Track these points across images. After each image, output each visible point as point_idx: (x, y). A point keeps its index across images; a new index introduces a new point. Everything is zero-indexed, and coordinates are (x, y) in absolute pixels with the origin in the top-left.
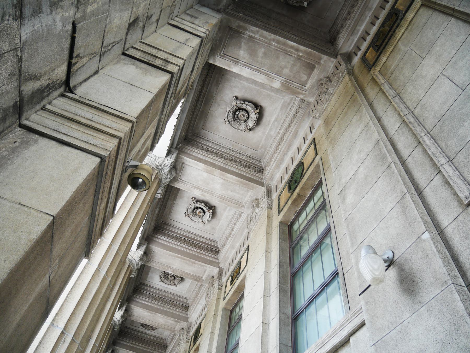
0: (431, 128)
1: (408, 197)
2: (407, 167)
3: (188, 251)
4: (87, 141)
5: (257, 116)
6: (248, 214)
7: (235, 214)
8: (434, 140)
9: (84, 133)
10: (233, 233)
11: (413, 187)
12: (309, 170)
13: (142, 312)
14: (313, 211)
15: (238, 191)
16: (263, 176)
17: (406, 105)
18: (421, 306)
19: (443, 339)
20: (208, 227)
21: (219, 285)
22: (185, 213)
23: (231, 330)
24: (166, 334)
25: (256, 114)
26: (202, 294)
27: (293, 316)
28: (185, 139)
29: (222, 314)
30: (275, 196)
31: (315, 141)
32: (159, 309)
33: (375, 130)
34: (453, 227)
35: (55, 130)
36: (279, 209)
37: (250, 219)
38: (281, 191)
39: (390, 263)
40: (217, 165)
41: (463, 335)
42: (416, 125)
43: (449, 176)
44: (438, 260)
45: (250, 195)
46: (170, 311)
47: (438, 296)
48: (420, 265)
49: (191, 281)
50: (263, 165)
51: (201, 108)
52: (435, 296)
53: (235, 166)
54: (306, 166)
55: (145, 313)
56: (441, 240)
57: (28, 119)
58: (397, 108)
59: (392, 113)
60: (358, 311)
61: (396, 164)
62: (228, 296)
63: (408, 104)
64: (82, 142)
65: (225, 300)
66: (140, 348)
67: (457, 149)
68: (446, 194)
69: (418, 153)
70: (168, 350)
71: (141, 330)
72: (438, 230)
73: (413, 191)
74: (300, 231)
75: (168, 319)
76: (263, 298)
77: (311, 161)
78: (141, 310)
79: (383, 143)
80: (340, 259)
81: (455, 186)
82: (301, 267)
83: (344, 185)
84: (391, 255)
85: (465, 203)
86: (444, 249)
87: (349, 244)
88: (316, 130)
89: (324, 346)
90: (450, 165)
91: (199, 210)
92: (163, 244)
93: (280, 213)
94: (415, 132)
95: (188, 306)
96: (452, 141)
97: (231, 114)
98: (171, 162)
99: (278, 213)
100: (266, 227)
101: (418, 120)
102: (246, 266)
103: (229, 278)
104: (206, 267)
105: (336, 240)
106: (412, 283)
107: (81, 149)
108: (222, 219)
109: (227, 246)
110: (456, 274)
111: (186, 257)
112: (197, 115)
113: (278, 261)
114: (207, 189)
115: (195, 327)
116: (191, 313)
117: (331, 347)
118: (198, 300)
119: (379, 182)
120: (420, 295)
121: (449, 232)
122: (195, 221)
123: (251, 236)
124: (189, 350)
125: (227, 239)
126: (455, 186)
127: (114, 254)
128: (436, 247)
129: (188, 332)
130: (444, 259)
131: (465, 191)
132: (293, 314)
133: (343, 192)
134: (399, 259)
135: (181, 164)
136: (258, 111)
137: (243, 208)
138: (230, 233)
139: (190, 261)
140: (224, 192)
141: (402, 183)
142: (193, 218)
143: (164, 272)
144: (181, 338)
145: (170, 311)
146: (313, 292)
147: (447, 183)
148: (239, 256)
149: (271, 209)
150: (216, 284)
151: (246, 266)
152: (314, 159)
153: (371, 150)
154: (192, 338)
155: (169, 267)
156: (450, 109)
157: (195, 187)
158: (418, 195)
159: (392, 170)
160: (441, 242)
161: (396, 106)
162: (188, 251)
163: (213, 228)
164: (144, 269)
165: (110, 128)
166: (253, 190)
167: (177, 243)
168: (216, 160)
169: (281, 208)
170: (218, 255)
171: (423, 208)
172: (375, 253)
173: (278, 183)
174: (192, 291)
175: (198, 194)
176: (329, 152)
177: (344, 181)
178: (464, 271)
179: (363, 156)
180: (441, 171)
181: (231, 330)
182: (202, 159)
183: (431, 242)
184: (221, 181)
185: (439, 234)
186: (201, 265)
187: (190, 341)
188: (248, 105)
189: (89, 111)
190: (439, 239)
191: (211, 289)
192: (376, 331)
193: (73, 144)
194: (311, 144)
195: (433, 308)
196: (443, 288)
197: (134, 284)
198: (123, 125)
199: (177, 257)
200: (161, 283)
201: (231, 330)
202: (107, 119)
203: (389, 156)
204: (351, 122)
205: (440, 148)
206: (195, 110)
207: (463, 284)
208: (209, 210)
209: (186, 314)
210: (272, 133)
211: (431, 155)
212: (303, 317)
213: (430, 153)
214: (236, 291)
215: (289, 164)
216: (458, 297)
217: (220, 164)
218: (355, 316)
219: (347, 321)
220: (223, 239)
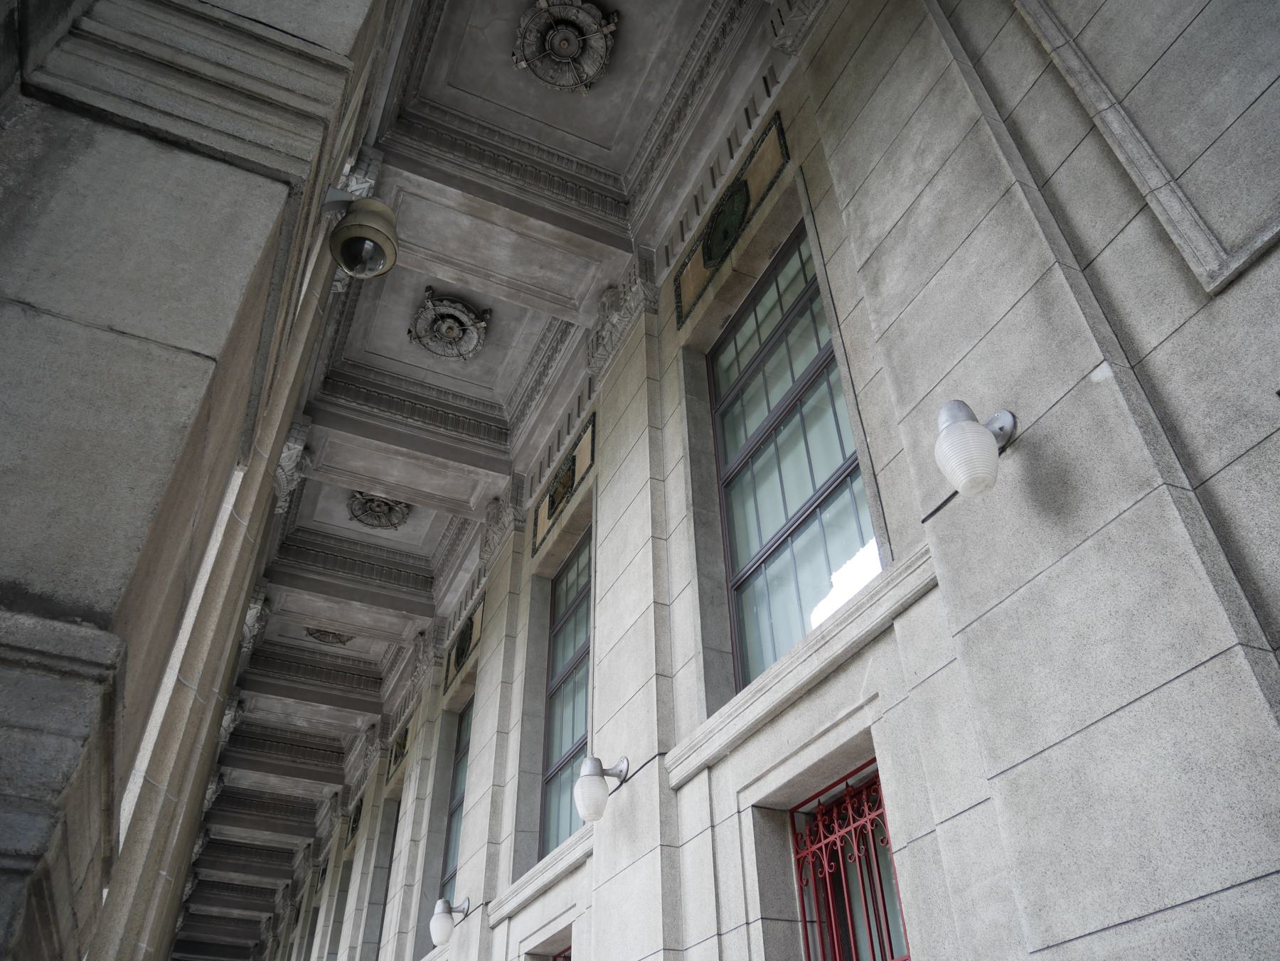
0: (1127, 87)
1: (1059, 275)
2: (1053, 195)
4: (237, 134)
5: (609, 43)
6: (587, 329)
7: (548, 330)
8: (1133, 121)
9: (220, 110)
10: (546, 381)
11: (1069, 250)
12: (764, 202)
14: (778, 315)
15: (559, 266)
16: (627, 220)
17: (1057, 17)
18: (1084, 538)
19: (1132, 609)
20: (475, 368)
21: (515, 520)
22: (410, 332)
23: (557, 629)
24: (377, 650)
25: (606, 36)
27: (733, 582)
28: (399, 117)
30: (664, 276)
31: (779, 118)
33: (968, 90)
34: (1170, 351)
35: (135, 102)
36: (678, 313)
37: (595, 342)
38: (681, 263)
39: (1007, 441)
41: (1182, 597)
42: (1086, 77)
43: (1170, 221)
44: (1130, 430)
45: (594, 277)
46: (384, 592)
47: (1127, 513)
48: (1084, 445)
49: (435, 512)
51: (442, 19)
52: (1120, 515)
53: (550, 193)
54: (755, 189)
55: (319, 604)
56: (1137, 382)
57: (42, 67)
58: (1033, 27)
59: (1016, 40)
60: (918, 559)
61: (1026, 188)
62: (543, 544)
63: (1063, 16)
64: (224, 138)
65: (536, 556)
66: (312, 688)
67: (1196, 148)
68: (1157, 267)
69: (1088, 156)
70: (385, 689)
71: (310, 645)
72: (1130, 358)
73: (1070, 260)
74: (742, 369)
77: (769, 178)
78: (307, 597)
79: (992, 129)
80: (863, 438)
81: (1185, 246)
82: (747, 463)
83: (875, 245)
84: (1007, 422)
85: (1208, 290)
86: (1144, 405)
87: (893, 398)
88: (783, 88)
89: (827, 645)
90: (1173, 191)
91: (450, 322)
92: (352, 420)
93: (683, 323)
94: (1082, 100)
95: (433, 578)
96: (1183, 125)
97: (532, 38)
98: (366, 185)
99: (678, 323)
100: (645, 363)
101: (1090, 63)
102: (591, 466)
103: (542, 500)
104: (478, 474)
105: (851, 389)
106: (1062, 487)
107: (227, 158)
108: (514, 344)
109: (532, 417)
110: (1171, 461)
111: (420, 451)
112: (431, 40)
113: (684, 449)
114: (473, 262)
115: (456, 628)
116: (442, 594)
117: (846, 646)
118: (459, 561)
119: (979, 237)
120: (1081, 513)
121: (1159, 361)
123: (599, 387)
124: (446, 683)
125: (531, 398)
126: (1185, 246)
128: (1128, 400)
129: (438, 640)
130: (1144, 427)
131: (1208, 259)
132: (731, 578)
133: (874, 264)
134: (1029, 430)
135: (394, 192)
136: (612, 27)
137: (574, 313)
138: (539, 382)
139: (432, 462)
140: (520, 270)
141: (1044, 240)
143: (361, 493)
144: (421, 657)
145: (384, 592)
146: (784, 521)
147: (1163, 238)
148: (568, 440)
149: (656, 312)
150: (508, 518)
151: (591, 466)
152: (780, 171)
153: (953, 145)
154: (450, 655)
155: (375, 481)
156: (1184, 34)
157: (438, 258)
158: (1083, 271)
159: (1015, 204)
160: (1138, 386)
161: (1029, 19)
162: (424, 435)
165: (288, 90)
166: (601, 261)
167: (393, 415)
168: (496, 179)
169: (685, 309)
171: (1095, 303)
172: (973, 418)
173: (671, 241)
175: (445, 276)
176: (827, 151)
177: (874, 232)
178: (1189, 455)
179: (930, 163)
180: (1149, 207)
181: (560, 625)
182: (455, 177)
183: (1117, 388)
184: (512, 238)
185: (1132, 368)
186: (462, 470)
187: (445, 663)
188: (583, 9)
189: (213, 36)
190: (1133, 381)
191: (495, 530)
192: (968, 601)
193: (200, 144)
194: (770, 129)
195: (1113, 542)
196: (1140, 496)
197: (280, 531)
198: (323, 82)
199: (397, 453)
200: (355, 525)
201: (557, 629)
202: (272, 63)
203: (1007, 164)
204: (895, 65)
205: (1150, 144)
206: (424, 25)
207: (1186, 484)
209: (428, 598)
210: (652, 95)
211: (1124, 164)
212: (759, 582)
213: (1122, 158)
214: (566, 531)
215: (702, 187)
216: (1177, 513)
218: (909, 572)
219: (888, 583)
220: (517, 399)
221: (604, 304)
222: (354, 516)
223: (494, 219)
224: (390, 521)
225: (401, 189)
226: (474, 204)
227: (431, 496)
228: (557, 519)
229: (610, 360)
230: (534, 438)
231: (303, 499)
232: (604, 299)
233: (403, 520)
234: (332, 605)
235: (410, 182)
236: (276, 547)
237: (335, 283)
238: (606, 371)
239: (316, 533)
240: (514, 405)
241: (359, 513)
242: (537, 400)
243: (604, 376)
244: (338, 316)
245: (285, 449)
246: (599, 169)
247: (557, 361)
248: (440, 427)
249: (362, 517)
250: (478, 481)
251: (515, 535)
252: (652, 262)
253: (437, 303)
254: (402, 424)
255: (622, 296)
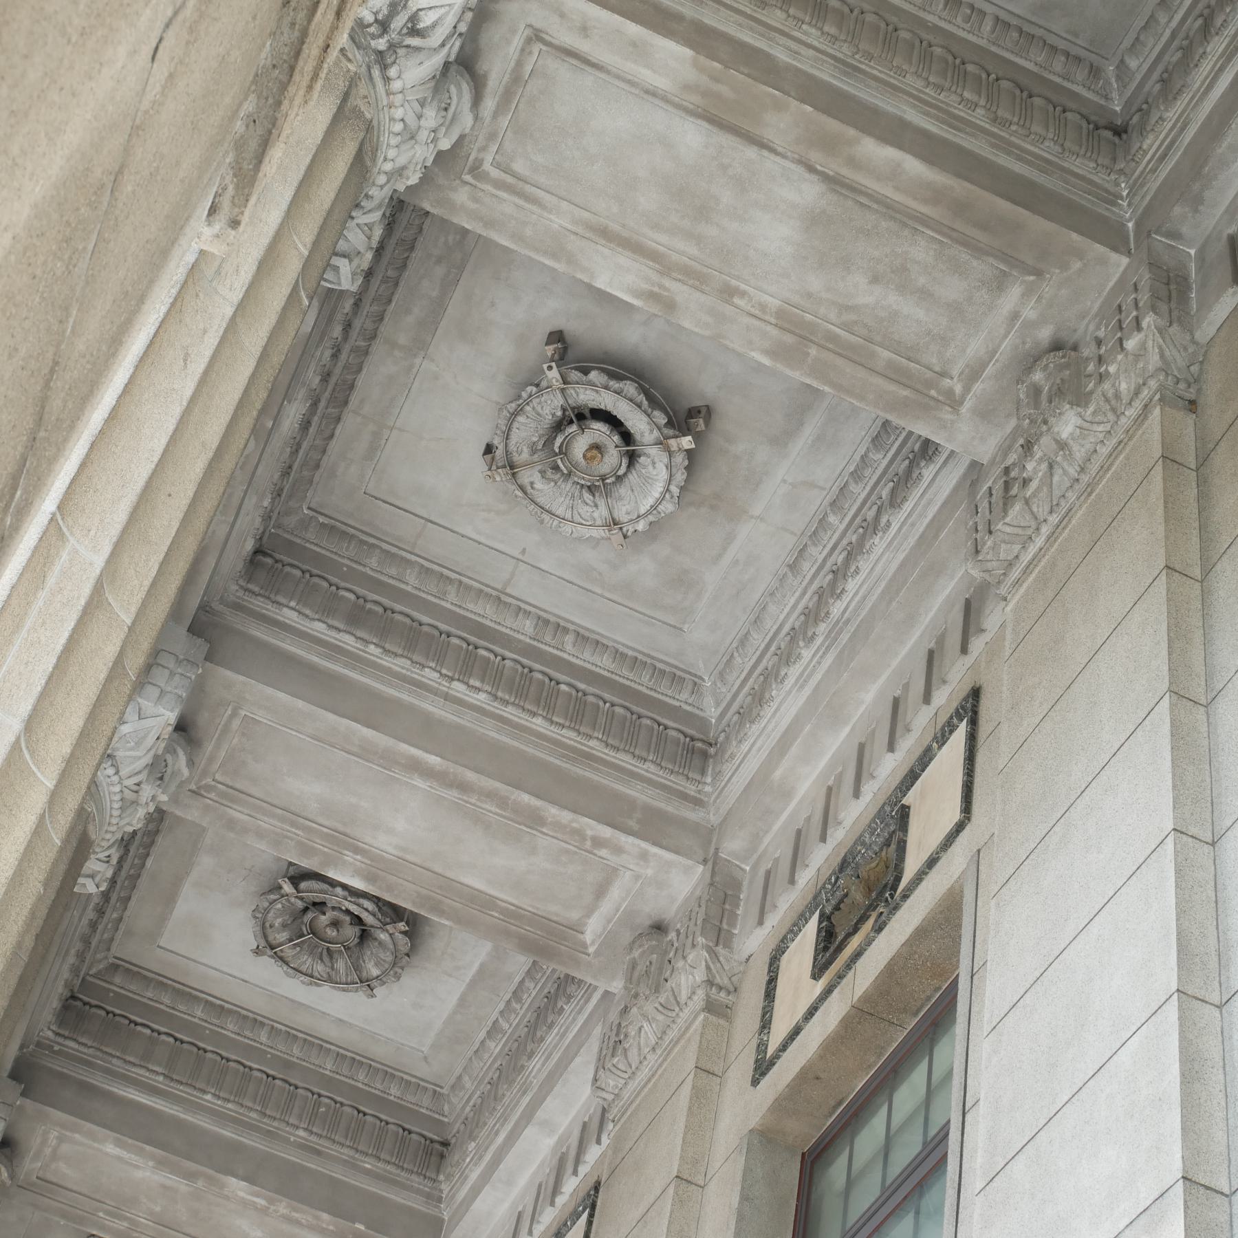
3: (491, 732)
7: (856, 475)
10: (837, 608)
13: (119, 1158)
15: (922, 281)
21: (710, 983)
22: (489, 449)
26: (556, 1057)
29: (747, 1171)
32: (237, 1148)
40: (788, 67)
45: (1015, 316)
50: (1115, 95)
53: (919, 84)
55: (139, 1174)
65: (763, 1083)
75: (298, 1223)
76: (1172, 1011)
78: (110, 1149)
91: (599, 430)
92: (312, 669)
102: (959, 827)
103: (794, 929)
104: (618, 850)
108: (757, 510)
118: (526, 1100)
122: (560, 512)
123: (995, 618)
125: (787, 657)
127: (83, 602)
135: (517, 41)
137: (946, 414)
138: (813, 615)
139: (503, 802)
140: (815, 283)
142: (543, 489)
148: (889, 767)
151: (959, 827)
155: (343, 841)
163: (683, 581)
164: (149, 862)
166: (1039, 273)
170: (703, 772)
174: (482, 1034)
184: (809, 192)
186: (579, 833)
197: (71, 959)
199: (415, 767)
200: (267, 972)
208: (671, 432)
209: (428, 1196)
214: (862, 1013)
217: (807, 63)
220: (744, 663)
221: (1036, 391)
222: (268, 947)
223: (769, 134)
224: (358, 968)
225: (537, 36)
226: (724, 90)
227: (484, 902)
228: (840, 977)
229: (1040, 541)
230: (786, 763)
231: (143, 883)
232: (1038, 376)
233: (397, 966)
234: (173, 1180)
235: (562, 15)
236: (55, 1004)
237: (336, 261)
238: (1027, 571)
239: (160, 983)
240: (735, 679)
241: (282, 936)
242: (804, 661)
243: (1018, 582)
244: (317, 379)
245: (131, 714)
246: (1052, 40)
247: (873, 557)
248: (534, 714)
249: (288, 951)
250: (615, 870)
251: (706, 1019)
252: (1186, 279)
253: (575, 375)
254: (435, 692)
255: (1091, 367)
